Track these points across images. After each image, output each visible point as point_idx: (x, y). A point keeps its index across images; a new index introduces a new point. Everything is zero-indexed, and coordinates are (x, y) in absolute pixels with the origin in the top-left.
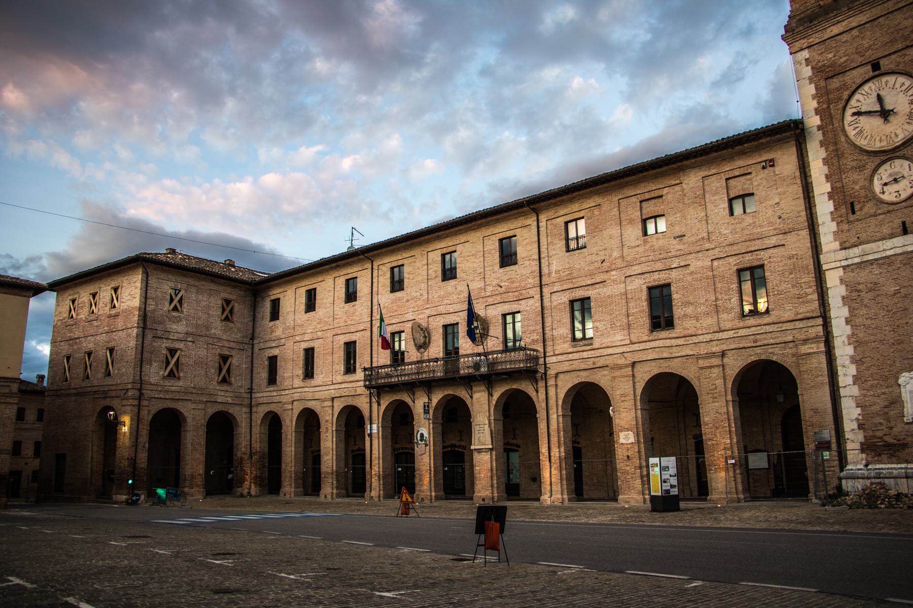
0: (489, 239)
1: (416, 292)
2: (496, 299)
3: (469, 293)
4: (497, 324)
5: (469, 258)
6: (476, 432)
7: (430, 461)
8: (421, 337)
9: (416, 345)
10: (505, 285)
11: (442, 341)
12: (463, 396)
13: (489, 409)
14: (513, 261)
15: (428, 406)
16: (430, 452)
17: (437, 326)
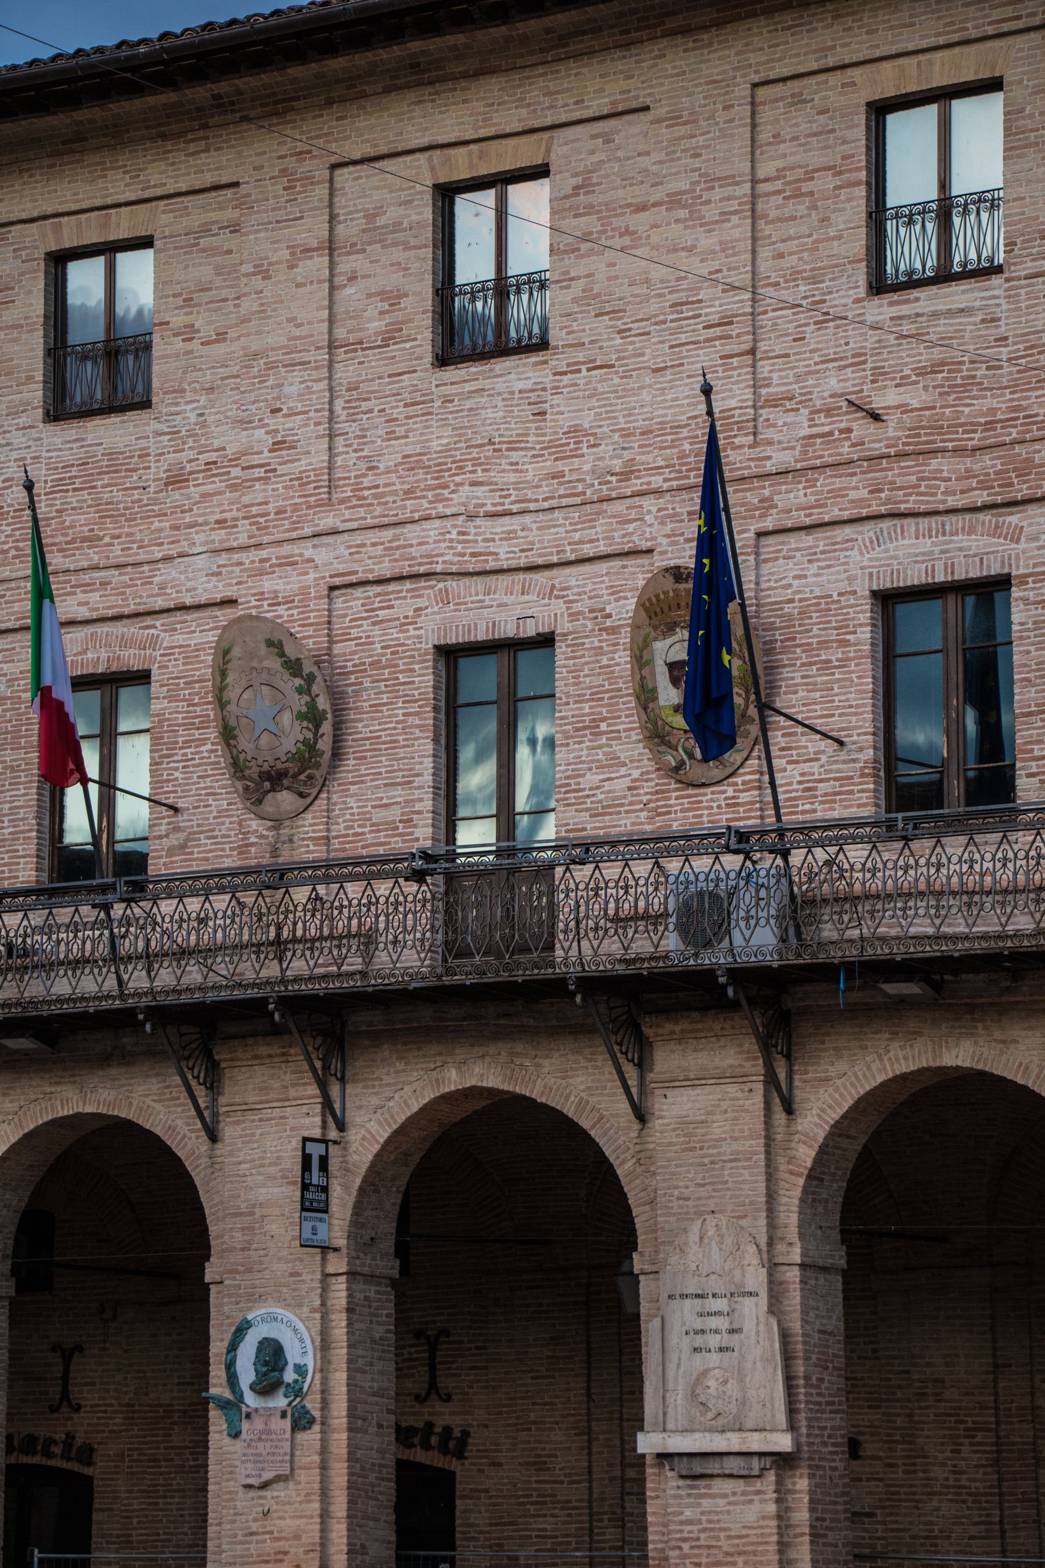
0: (798, 100)
1: (245, 423)
2: (837, 494)
3: (713, 427)
4: (835, 655)
5: (640, 221)
6: (680, 1343)
7: (324, 1530)
8: (286, 718)
9: (237, 768)
10: (905, 408)
11: (429, 747)
12: (581, 1104)
13: (771, 1196)
14: (124, 385)
15: (324, 1161)
16: (324, 1467)
17: (394, 649)
